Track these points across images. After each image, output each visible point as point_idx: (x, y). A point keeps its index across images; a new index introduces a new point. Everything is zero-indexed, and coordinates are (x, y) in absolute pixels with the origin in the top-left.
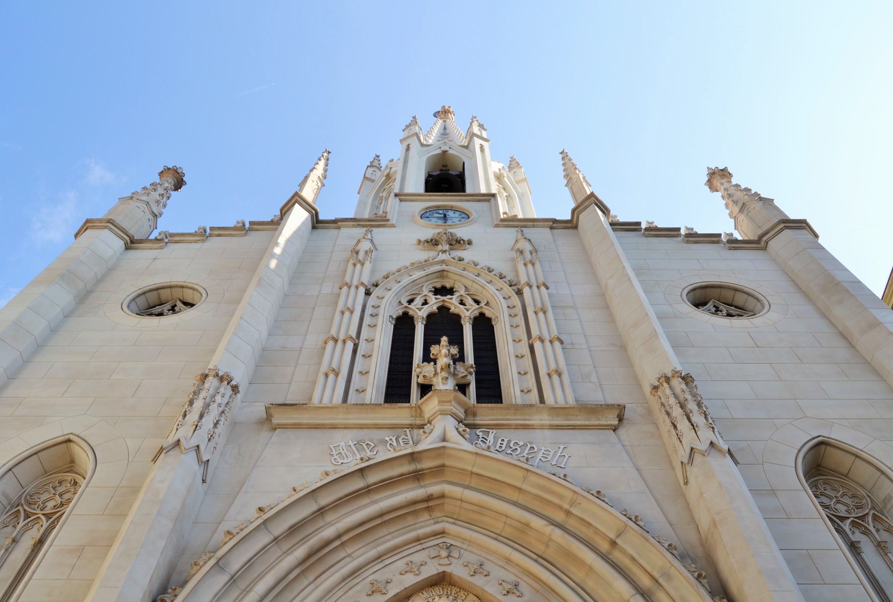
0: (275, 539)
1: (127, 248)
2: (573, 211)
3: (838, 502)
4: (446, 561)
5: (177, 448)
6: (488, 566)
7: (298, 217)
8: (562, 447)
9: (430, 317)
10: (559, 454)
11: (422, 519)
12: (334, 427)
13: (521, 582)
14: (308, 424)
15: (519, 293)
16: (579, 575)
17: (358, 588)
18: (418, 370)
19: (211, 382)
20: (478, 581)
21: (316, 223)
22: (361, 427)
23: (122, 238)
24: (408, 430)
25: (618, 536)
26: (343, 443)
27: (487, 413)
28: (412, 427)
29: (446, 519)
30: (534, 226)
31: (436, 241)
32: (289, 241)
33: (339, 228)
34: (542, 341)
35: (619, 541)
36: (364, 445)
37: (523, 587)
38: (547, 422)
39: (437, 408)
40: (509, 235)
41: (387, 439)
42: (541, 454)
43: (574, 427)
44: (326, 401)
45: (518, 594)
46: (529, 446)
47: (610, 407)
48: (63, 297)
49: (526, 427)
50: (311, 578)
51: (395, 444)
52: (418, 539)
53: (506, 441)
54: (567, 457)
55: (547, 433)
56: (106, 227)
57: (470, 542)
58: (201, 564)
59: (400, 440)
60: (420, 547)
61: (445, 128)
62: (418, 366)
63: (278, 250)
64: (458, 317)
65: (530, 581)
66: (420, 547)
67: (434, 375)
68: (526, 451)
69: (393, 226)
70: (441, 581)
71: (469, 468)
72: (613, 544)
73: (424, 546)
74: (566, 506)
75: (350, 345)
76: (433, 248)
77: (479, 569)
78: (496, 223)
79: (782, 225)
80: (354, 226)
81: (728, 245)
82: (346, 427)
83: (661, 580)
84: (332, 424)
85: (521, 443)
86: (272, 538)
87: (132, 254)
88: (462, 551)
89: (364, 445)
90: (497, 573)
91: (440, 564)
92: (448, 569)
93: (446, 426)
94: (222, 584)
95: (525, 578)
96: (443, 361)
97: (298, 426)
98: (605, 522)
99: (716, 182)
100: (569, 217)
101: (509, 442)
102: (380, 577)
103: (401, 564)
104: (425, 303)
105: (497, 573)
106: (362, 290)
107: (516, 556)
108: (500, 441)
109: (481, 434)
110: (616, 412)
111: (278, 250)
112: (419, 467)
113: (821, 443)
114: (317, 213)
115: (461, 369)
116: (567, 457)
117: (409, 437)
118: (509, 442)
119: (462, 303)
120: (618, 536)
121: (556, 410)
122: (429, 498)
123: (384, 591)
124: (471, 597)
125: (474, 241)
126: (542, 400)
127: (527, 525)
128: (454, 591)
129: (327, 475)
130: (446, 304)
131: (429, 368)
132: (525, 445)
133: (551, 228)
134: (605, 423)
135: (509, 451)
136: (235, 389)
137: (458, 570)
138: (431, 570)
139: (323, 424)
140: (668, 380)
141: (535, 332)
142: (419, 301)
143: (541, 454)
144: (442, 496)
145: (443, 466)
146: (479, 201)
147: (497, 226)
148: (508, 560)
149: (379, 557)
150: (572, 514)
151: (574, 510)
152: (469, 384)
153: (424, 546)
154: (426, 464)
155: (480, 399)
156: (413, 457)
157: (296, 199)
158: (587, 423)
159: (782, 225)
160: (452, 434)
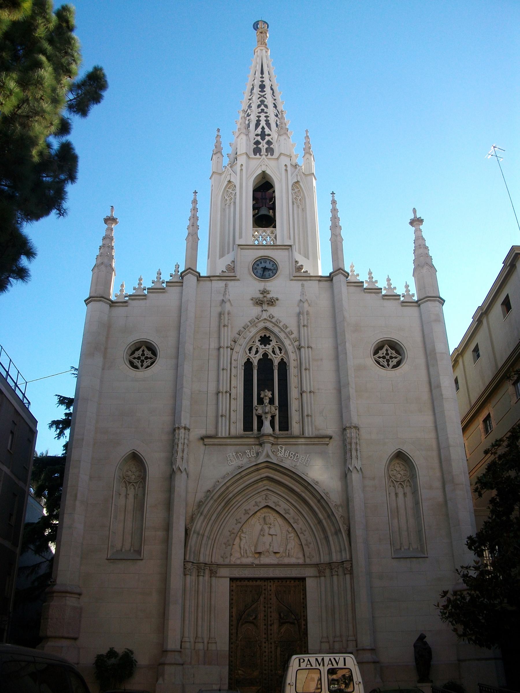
26: (231, 454)
109: (279, 448)
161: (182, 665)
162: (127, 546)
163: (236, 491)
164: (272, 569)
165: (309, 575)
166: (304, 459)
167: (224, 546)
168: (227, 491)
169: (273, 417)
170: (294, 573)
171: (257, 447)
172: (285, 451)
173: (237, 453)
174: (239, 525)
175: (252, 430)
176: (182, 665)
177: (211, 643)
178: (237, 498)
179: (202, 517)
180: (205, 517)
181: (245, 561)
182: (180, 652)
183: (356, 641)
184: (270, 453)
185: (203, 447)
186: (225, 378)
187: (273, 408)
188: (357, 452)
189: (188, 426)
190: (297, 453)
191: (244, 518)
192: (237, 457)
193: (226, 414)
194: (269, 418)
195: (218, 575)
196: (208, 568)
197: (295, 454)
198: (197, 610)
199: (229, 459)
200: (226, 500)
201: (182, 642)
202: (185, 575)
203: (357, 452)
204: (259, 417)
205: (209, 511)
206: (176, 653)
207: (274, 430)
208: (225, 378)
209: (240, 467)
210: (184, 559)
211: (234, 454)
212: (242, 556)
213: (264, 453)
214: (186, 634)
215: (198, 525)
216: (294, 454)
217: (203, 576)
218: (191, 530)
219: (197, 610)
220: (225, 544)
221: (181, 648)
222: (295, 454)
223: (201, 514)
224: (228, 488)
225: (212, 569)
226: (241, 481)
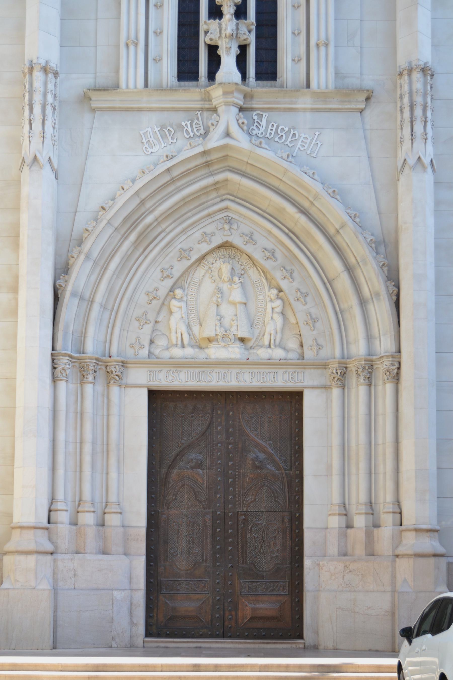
0: (116, 229)
5: (36, 163)
6: (256, 236)
8: (317, 133)
10: (314, 142)
12: (140, 110)
13: (277, 250)
14: (120, 108)
16: (313, 248)
17: (171, 254)
19: (38, 75)
22: (162, 110)
24: (199, 113)
25: (341, 228)
26: (149, 130)
27: (262, 91)
28: (202, 110)
29: (229, 197)
35: (341, 231)
36: (166, 131)
37: (278, 254)
38: (309, 106)
39: (222, 100)
41: (183, 124)
44: (131, 85)
45: (274, 259)
46: (292, 132)
49: (291, 110)
50: (141, 250)
52: (209, 215)
53: (275, 125)
54: (319, 144)
55: (308, 115)
57: (245, 217)
58: (75, 257)
59: (193, 124)
60: (210, 220)
62: (205, 23)
66: (210, 220)
67: (219, 37)
71: (246, 160)
72: (338, 231)
73: (214, 219)
74: (311, 199)
77: (250, 239)
82: (150, 110)
83: (361, 264)
84: (139, 108)
86: (114, 229)
88: (239, 223)
89: (166, 131)
91: (224, 235)
92: (230, 239)
94: (90, 268)
95: (279, 246)
97: (112, 109)
101: (278, 127)
102: (185, 246)
103: (198, 235)
105: (263, 242)
107: (275, 231)
108: (270, 125)
109: (256, 118)
112: (209, 159)
115: (243, 25)
116: (319, 144)
117: (200, 122)
118: (278, 127)
120: (341, 228)
123: (189, 258)
126: (308, 86)
127: (284, 209)
128: (233, 252)
129: (144, 172)
131: (214, 24)
134: (354, 106)
135: (276, 139)
136: (56, 74)
137: (237, 241)
138: (218, 240)
139: (132, 108)
140: (410, 71)
144: (226, 180)
145: (227, 156)
148: (270, 233)
149: (184, 231)
150: (314, 205)
151: (315, 203)
152: (249, 44)
153: (214, 219)
154: (214, 156)
155: (259, 76)
156: (204, 153)
158: (340, 106)
160: (235, 129)
161: (52, 553)
162: (331, 85)
163: (157, 213)
164: (234, 371)
165: (310, 383)
166: (308, 141)
167: (136, 324)
168: (143, 210)
169: (243, 48)
170: (280, 381)
171: (206, 114)
172: (268, 122)
173: (163, 127)
174: (169, 283)
175: (195, 76)
176: (52, 553)
177: (110, 513)
178: (163, 226)
179: (90, 264)
180: (96, 263)
181: (177, 352)
182: (47, 529)
183: (400, 513)
184: (235, 129)
185: (87, 116)
186: (323, 70)
187: (243, 29)
188: (425, 127)
189: (53, 64)
190: (294, 128)
191: (179, 268)
192: (164, 137)
193: (137, 38)
194: (235, 51)
195: (124, 381)
196: (104, 368)
197: (289, 131)
198: (81, 449)
199: (144, 141)
200: (140, 228)
201: (50, 511)
202: (54, 379)
203: (425, 127)
204: (213, 50)
205: (103, 250)
206: (39, 532)
207: (244, 77)
208: (323, 70)
209: (169, 158)
210: (53, 349)
211: (156, 130)
212: (150, 381)
213: (221, 128)
214: (60, 495)
215: (79, 278)
216: (286, 129)
217: (94, 383)
218: (64, 290)
219: (81, 449)
220: (138, 319)
221: (49, 522)
222: (289, 131)
223: (87, 257)
224: (143, 202)
225: (110, 370)
226: (172, 188)
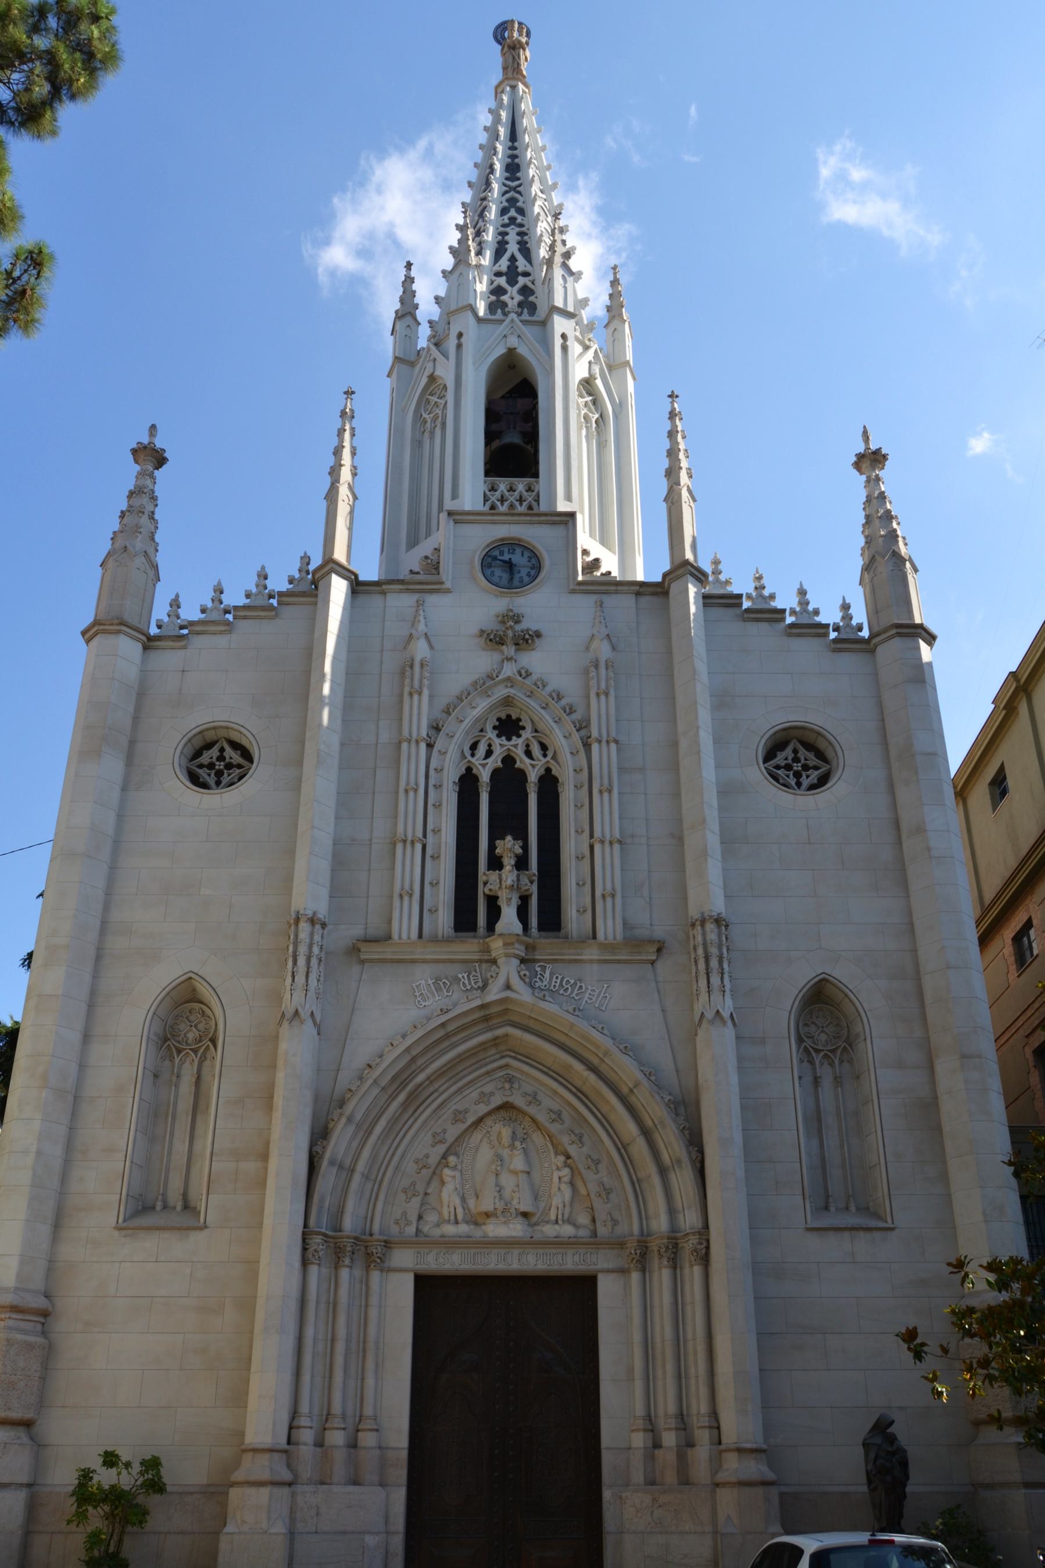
1: (146, 648)
2: (665, 575)
3: (822, 1031)
4: (508, 1093)
7: (339, 587)
9: (495, 773)
11: (490, 1053)
12: (414, 961)
13: (564, 1111)
15: (587, 746)
16: (605, 1109)
17: (444, 1117)
18: (484, 878)
19: (304, 926)
20: (532, 1110)
21: (357, 587)
23: (138, 640)
26: (423, 982)
27: (547, 945)
30: (616, 592)
31: (501, 638)
32: (335, 658)
33: (384, 593)
34: (602, 842)
35: (635, 1091)
37: (565, 1115)
38: (596, 957)
40: (585, 604)
42: (587, 995)
43: (618, 962)
44: (404, 936)
47: (651, 941)
48: (113, 766)
51: (467, 982)
55: (595, 967)
56: (119, 632)
61: (513, 157)
62: (485, 874)
63: (326, 690)
64: (522, 775)
65: (572, 1113)
68: (576, 992)
69: (448, 591)
70: (506, 1106)
71: (528, 1013)
72: (631, 1091)
75: (418, 847)
76: (497, 647)
77: (534, 1099)
78: (572, 587)
79: (894, 631)
80: (401, 591)
81: (833, 646)
82: (424, 961)
85: (572, 981)
87: (153, 655)
90: (547, 1102)
92: (510, 1099)
93: (509, 969)
96: (509, 862)
98: (627, 1070)
99: (865, 465)
100: (659, 579)
102: (460, 1107)
103: (475, 1095)
104: (489, 753)
106: (423, 746)
109: (538, 969)
110: (656, 947)
111: (326, 690)
112: (487, 1013)
113: (823, 980)
114: (356, 576)
119: (528, 754)
121: (605, 947)
122: (496, 1038)
124: (527, 1118)
125: (543, 632)
130: (512, 754)
131: (493, 876)
132: (575, 984)
133: (638, 594)
136: (324, 925)
137: (519, 1101)
138: (497, 1101)
140: (703, 922)
141: (597, 833)
142: (482, 749)
143: (587, 995)
144: (507, 1035)
146: (554, 523)
147: (573, 592)
148: (555, 1092)
149: (460, 1090)
151: (605, 1059)
152: (531, 895)
155: (541, 928)
156: (483, 1007)
157: (330, 566)
159: (894, 631)
160: (516, 982)
